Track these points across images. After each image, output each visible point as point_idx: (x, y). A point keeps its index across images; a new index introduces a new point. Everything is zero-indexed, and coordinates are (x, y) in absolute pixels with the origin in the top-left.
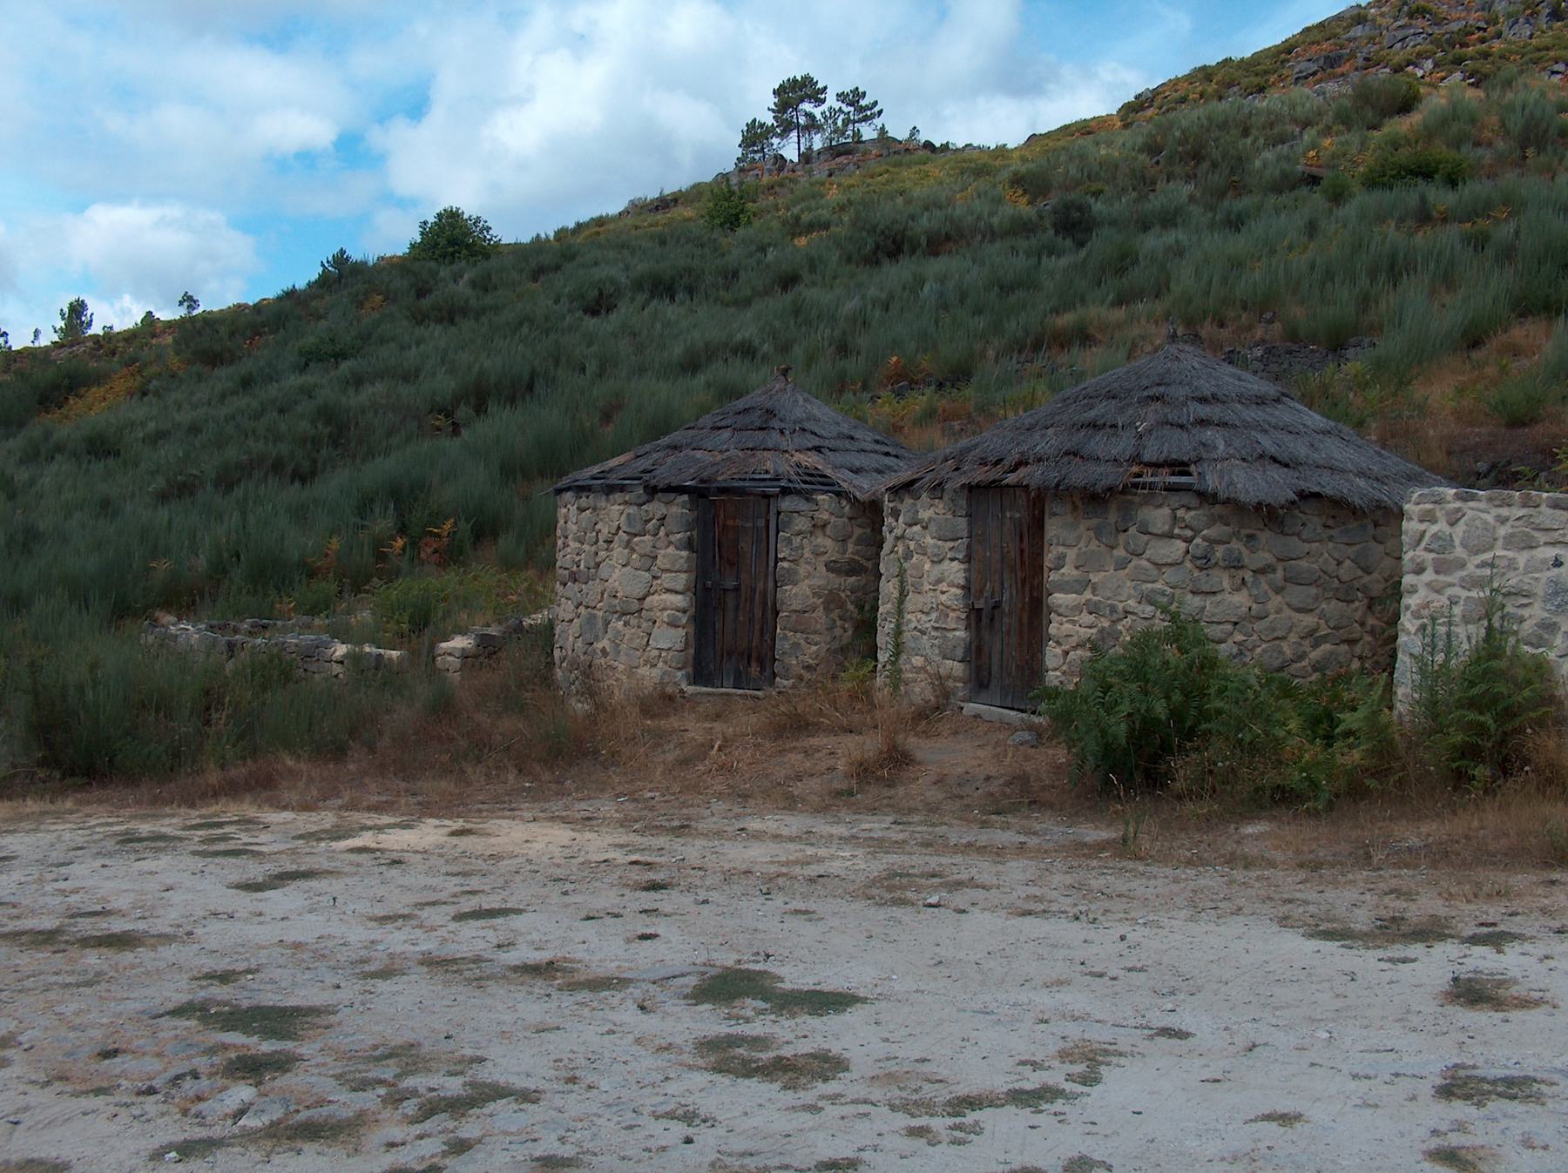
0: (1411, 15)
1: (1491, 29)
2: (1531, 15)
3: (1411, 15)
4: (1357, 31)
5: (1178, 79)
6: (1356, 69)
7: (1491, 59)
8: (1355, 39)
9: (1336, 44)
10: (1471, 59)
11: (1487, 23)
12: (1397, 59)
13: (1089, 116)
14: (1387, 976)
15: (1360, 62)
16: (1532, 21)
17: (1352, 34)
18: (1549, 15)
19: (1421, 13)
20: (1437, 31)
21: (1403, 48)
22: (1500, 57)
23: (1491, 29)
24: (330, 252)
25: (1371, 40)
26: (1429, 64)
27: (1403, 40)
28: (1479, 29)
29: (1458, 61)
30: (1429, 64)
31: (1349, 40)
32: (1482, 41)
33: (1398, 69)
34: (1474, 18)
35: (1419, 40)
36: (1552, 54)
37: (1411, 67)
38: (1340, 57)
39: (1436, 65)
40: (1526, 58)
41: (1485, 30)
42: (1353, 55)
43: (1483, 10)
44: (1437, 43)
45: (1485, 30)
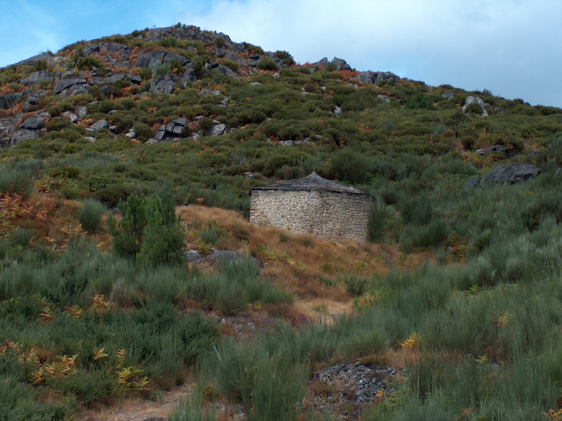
0: (81, 67)
1: (144, 83)
2: (177, 73)
3: (81, 67)
4: (35, 77)
5: (504, 99)
6: (24, 111)
7: (133, 109)
8: (32, 83)
9: (12, 87)
10: (117, 108)
11: (142, 78)
12: (58, 105)
13: (252, 44)
14: (36, 323)
15: (27, 105)
16: (176, 77)
17: (30, 79)
18: (191, 73)
19: (89, 65)
20: (99, 81)
21: (68, 94)
22: (141, 108)
23: (144, 83)
24: (325, 57)
25: (44, 86)
26: (83, 111)
27: (68, 87)
28: (134, 82)
29: (106, 110)
30: (83, 111)
31: (26, 84)
32: (134, 92)
33: (55, 114)
34: (134, 72)
35: (82, 88)
36: (179, 108)
37: (68, 112)
38: (13, 99)
39: (89, 112)
40: (160, 111)
41: (138, 83)
42: (24, 98)
43: (142, 65)
44: (95, 93)
45: (138, 83)
